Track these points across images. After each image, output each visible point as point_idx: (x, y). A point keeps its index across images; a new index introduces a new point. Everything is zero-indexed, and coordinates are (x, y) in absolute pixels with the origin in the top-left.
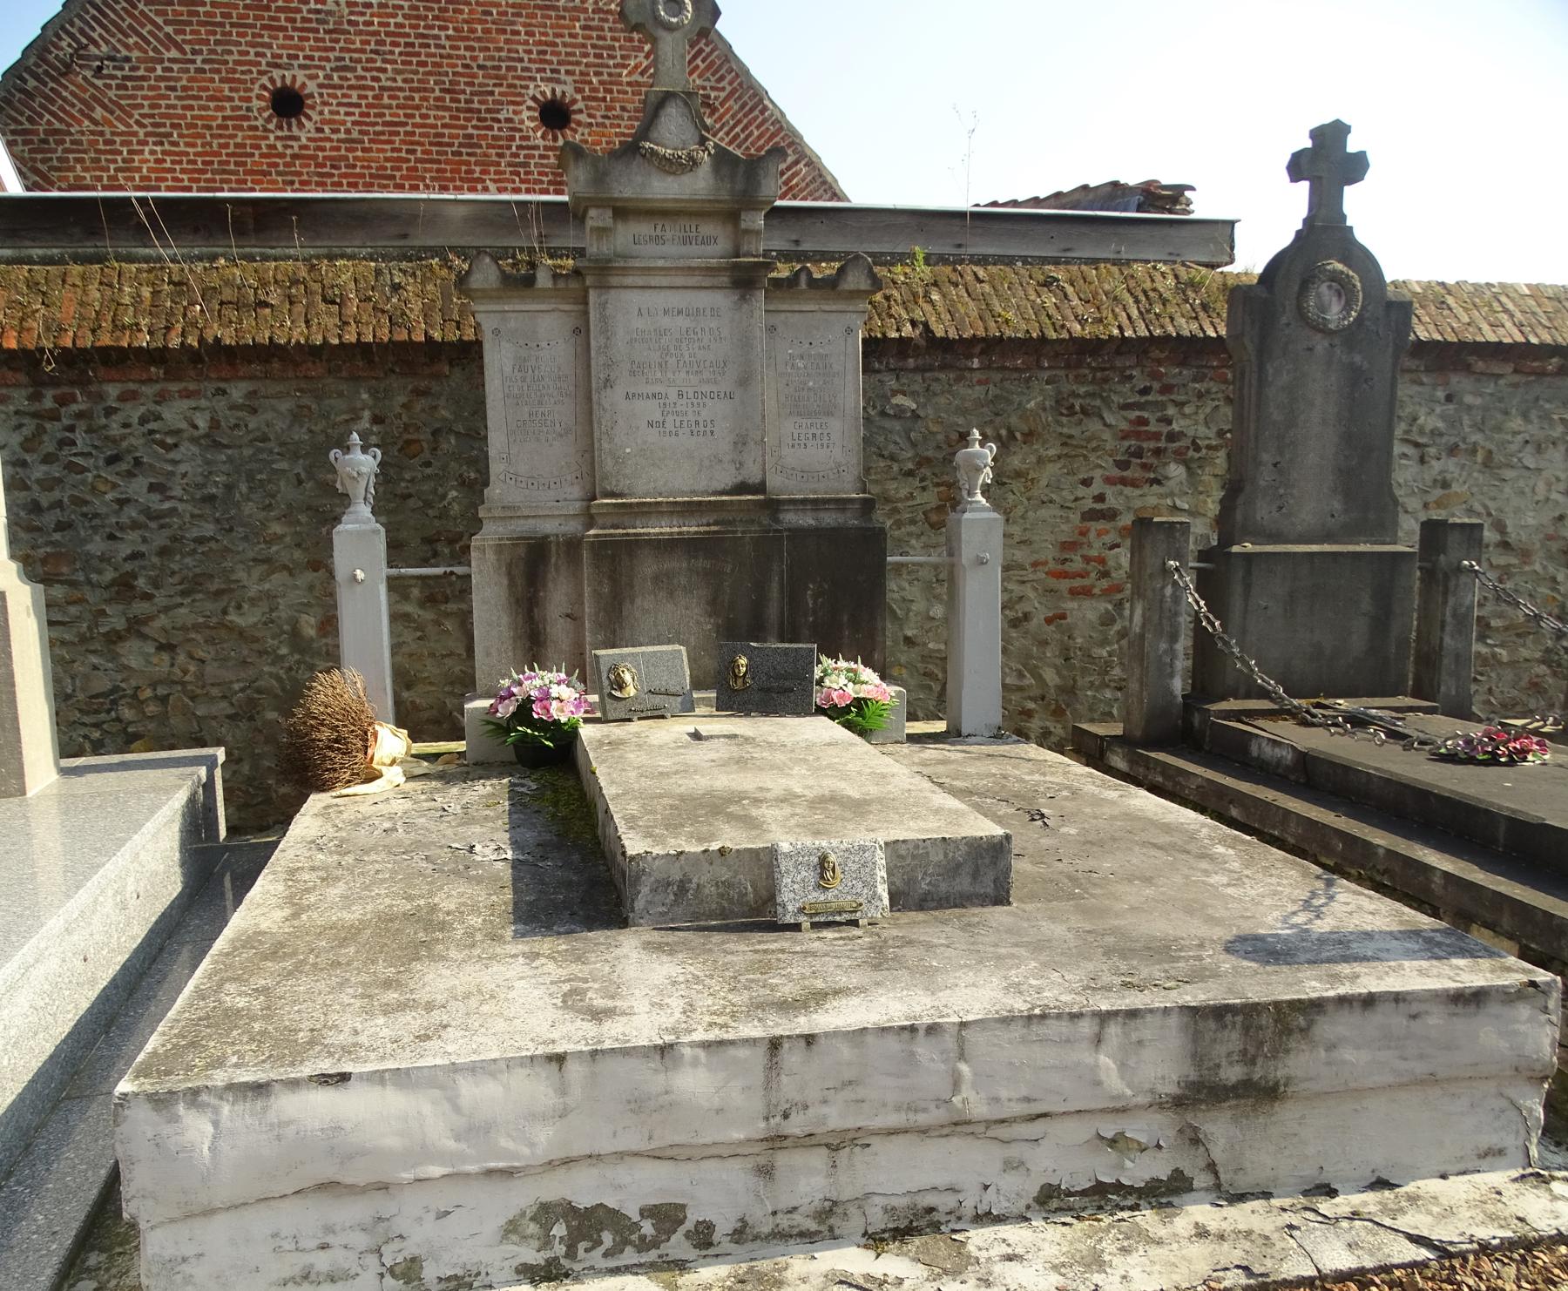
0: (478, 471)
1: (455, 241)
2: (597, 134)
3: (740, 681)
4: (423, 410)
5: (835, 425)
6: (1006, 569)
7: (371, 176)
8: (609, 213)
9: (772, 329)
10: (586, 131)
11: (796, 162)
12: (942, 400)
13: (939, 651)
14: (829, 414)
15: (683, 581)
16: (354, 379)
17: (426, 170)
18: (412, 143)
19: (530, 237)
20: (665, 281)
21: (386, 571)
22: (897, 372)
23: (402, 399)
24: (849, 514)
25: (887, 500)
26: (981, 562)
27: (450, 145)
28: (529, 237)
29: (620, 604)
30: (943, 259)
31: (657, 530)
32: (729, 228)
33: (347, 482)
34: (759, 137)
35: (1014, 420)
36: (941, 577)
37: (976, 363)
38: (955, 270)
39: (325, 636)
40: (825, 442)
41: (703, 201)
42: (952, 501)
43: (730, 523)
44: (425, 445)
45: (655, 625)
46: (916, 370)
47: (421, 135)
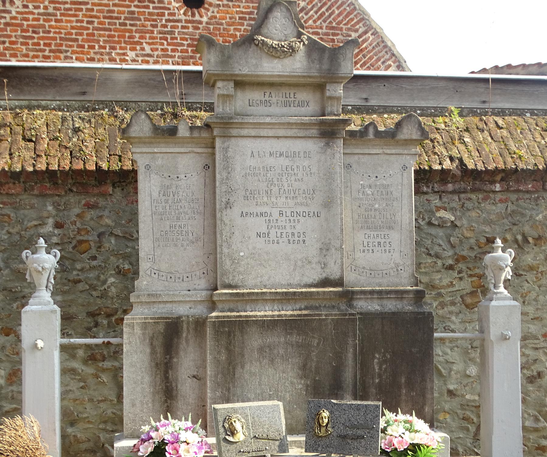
0: (131, 263)
1: (119, 97)
2: (223, 12)
3: (323, 429)
4: (92, 219)
5: (395, 236)
6: (524, 338)
7: (61, 39)
8: (232, 84)
9: (348, 166)
10: (216, 10)
11: (365, 32)
12: (473, 214)
13: (474, 401)
14: (390, 228)
15: (282, 351)
16: (42, 195)
17: (100, 35)
18: (91, 17)
19: (174, 94)
20: (271, 133)
21: (59, 340)
22: (440, 194)
23: (77, 211)
24: (405, 302)
25: (433, 287)
26: (505, 338)
27: (118, 18)
28: (173, 95)
29: (234, 369)
30: (472, 112)
31: (262, 313)
32: (318, 95)
33: (34, 274)
34: (339, 15)
35: (527, 229)
36: (475, 345)
37: (498, 187)
38: (481, 120)
39: (11, 384)
40: (387, 248)
41: (299, 77)
42: (482, 290)
43: (317, 308)
44: (92, 244)
45: (260, 384)
46: (454, 192)
47: (98, 11)
